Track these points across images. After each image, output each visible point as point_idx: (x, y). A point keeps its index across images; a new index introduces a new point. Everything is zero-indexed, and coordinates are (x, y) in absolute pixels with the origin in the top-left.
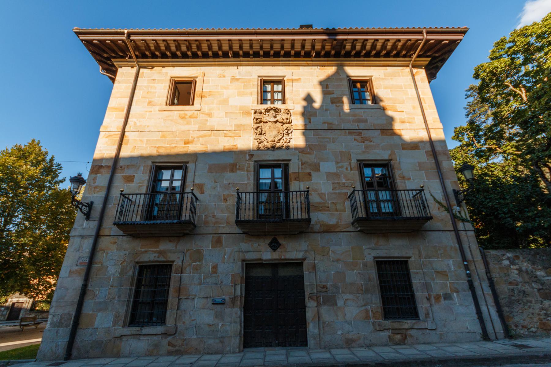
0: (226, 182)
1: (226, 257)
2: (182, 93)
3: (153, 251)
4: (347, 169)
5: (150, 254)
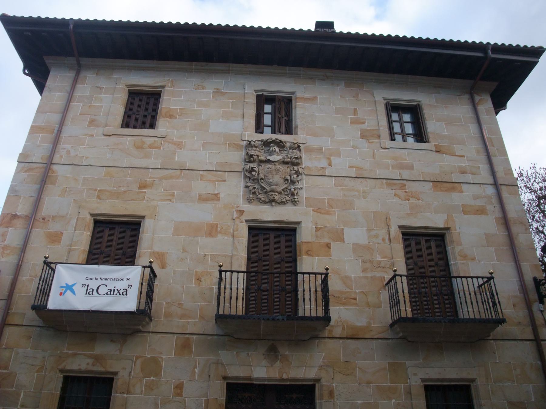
0: (201, 253)
1: (196, 371)
2: (142, 110)
3: (84, 355)
4: (383, 240)
5: (81, 363)
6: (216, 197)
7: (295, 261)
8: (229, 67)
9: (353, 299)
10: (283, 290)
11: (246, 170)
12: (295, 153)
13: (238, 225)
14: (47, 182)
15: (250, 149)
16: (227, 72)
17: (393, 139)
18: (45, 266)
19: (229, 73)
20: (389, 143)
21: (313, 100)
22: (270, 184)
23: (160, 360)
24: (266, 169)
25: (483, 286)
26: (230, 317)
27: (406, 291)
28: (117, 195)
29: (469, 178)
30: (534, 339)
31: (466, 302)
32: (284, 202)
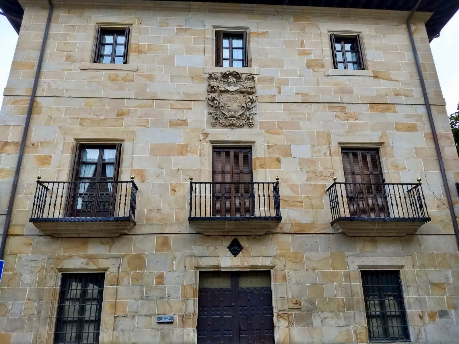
0: (174, 168)
1: (174, 263)
3: (79, 256)
4: (325, 154)
6: (185, 123)
7: (251, 173)
8: (190, 5)
9: (300, 202)
10: (242, 196)
13: (204, 145)
14: (33, 113)
16: (188, 10)
17: (336, 67)
18: (39, 185)
19: (190, 11)
20: (331, 71)
21: (265, 34)
22: (229, 111)
23: (144, 256)
24: (226, 98)
25: (412, 191)
26: (201, 219)
27: (345, 196)
28: (99, 122)
29: (403, 100)
30: (454, 233)
31: (397, 205)
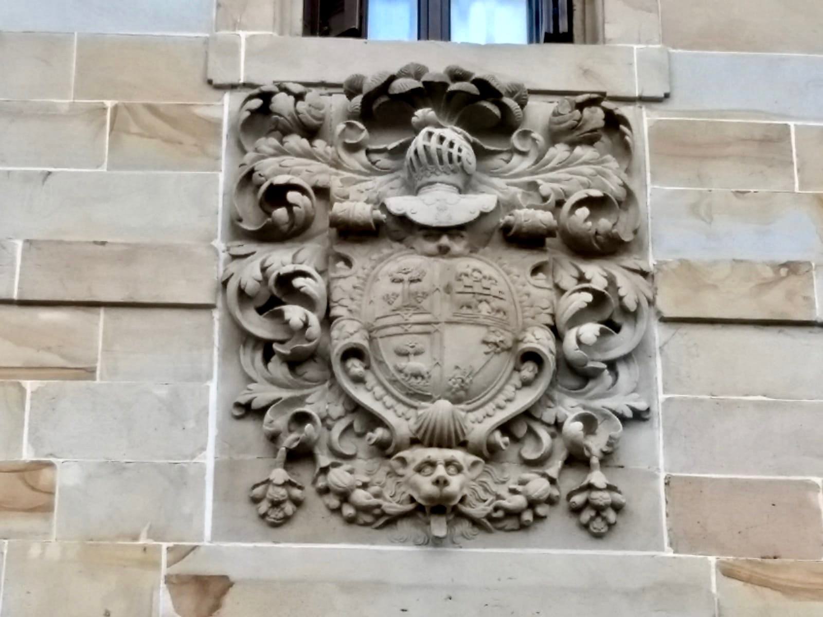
11: (243, 296)
12: (582, 172)
15: (268, 143)
22: (415, 392)
32: (513, 514)
